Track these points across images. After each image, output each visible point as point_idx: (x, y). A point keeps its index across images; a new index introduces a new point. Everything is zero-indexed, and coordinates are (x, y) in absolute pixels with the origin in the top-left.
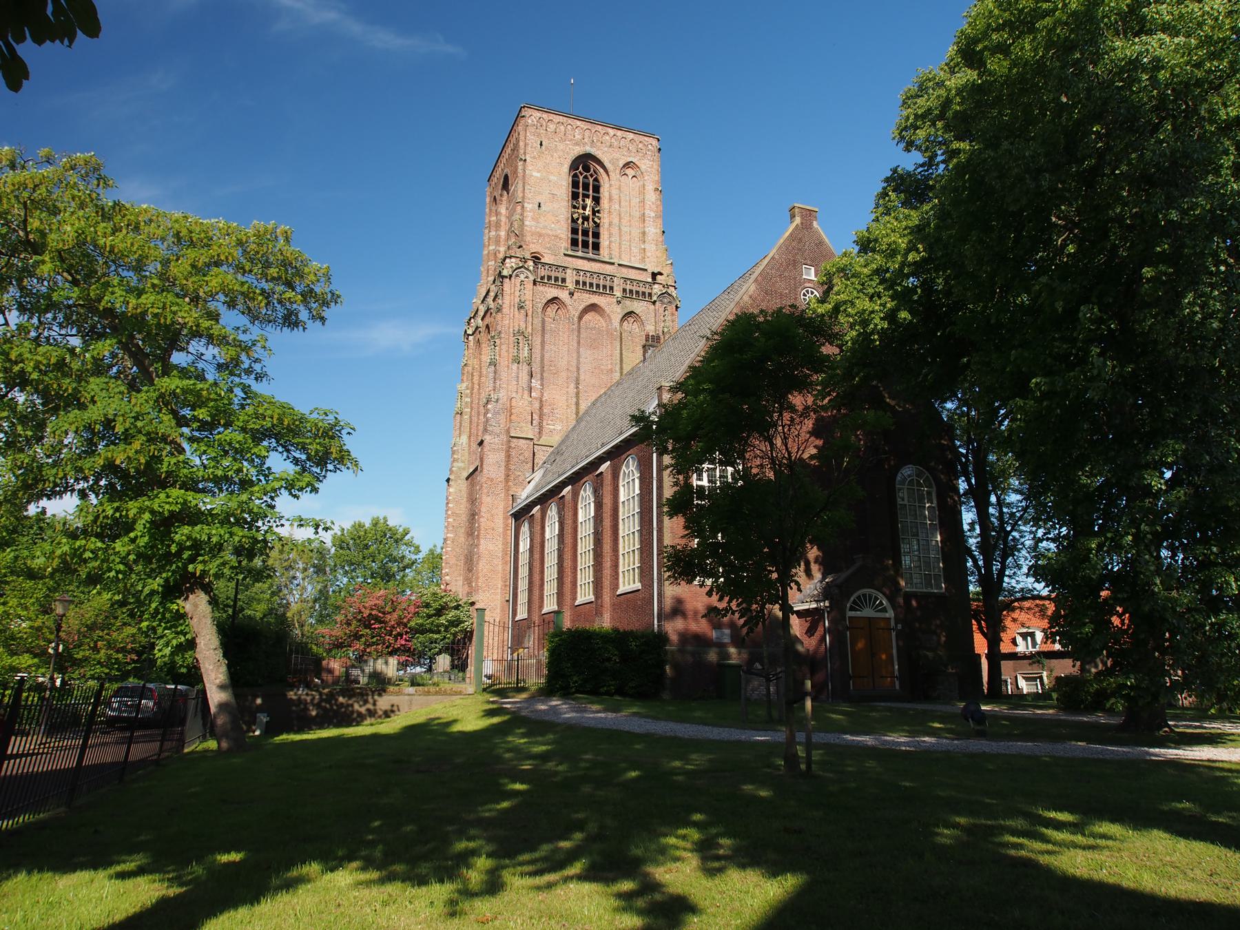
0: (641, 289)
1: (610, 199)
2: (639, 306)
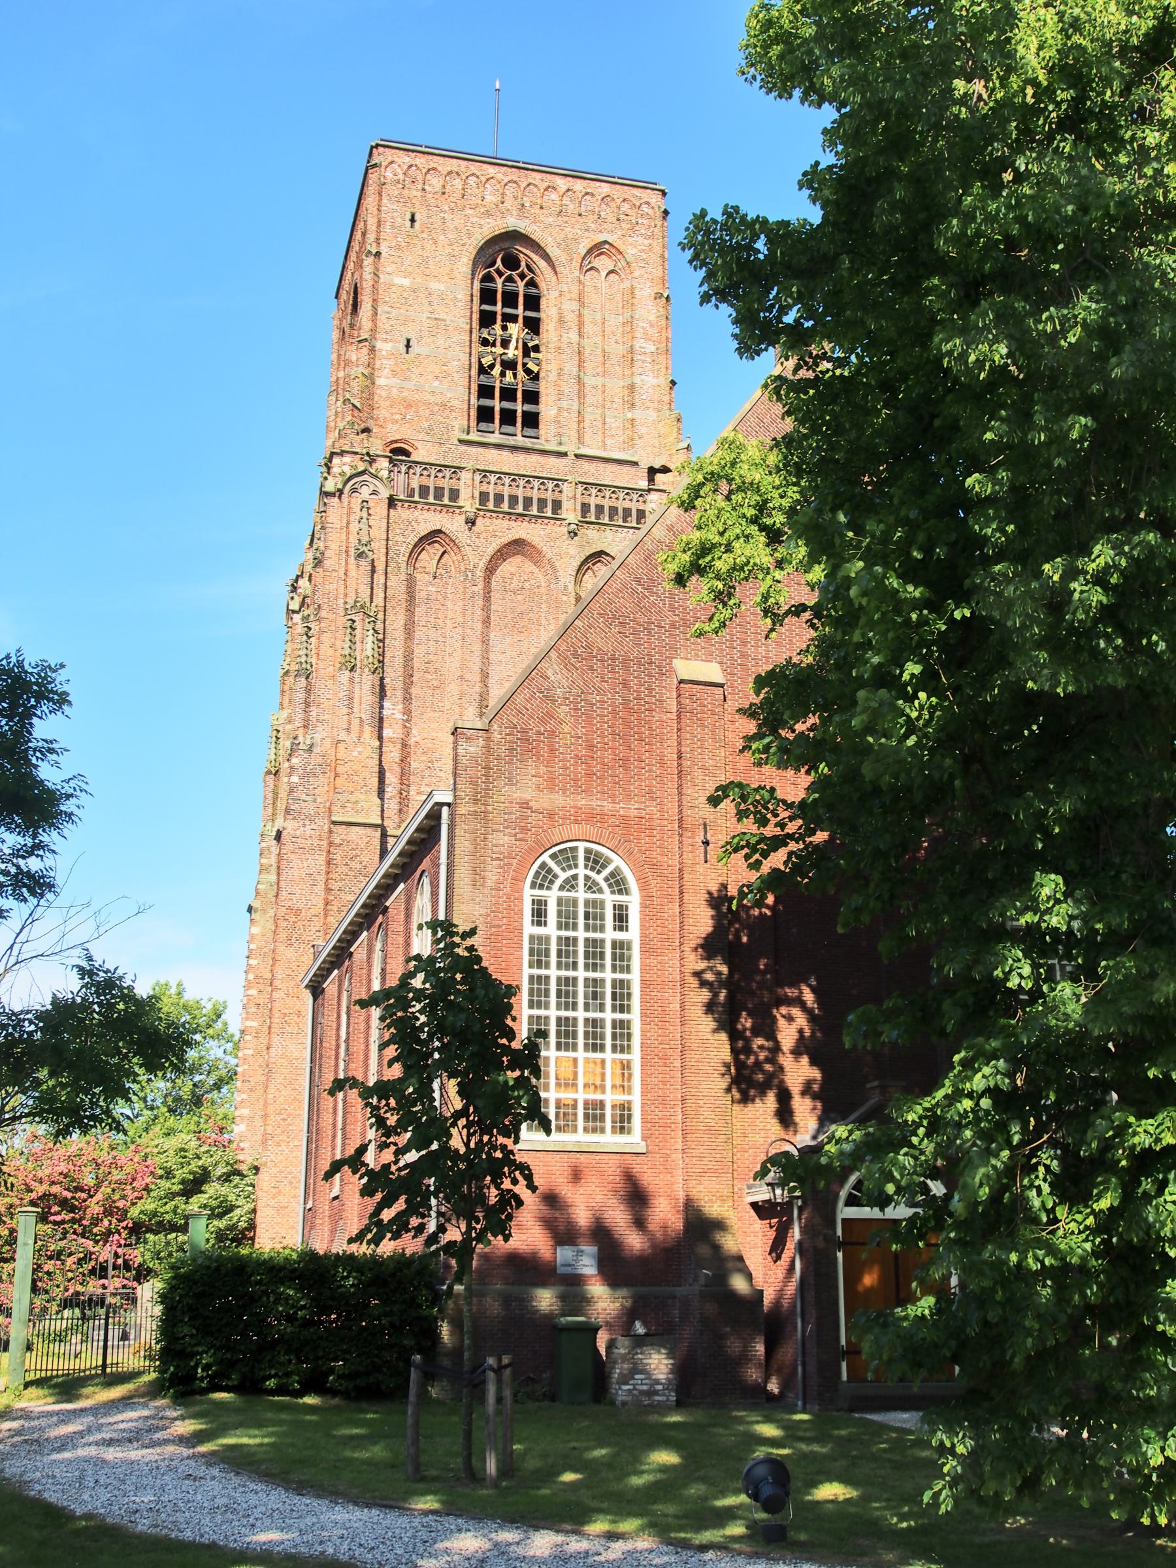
1: (561, 321)
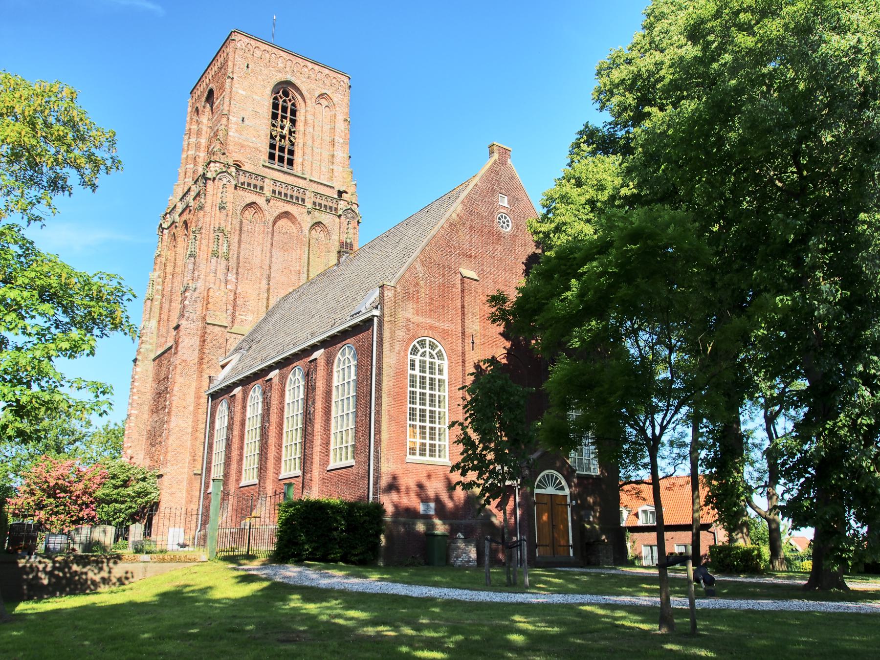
0: (329, 204)
2: (326, 218)
